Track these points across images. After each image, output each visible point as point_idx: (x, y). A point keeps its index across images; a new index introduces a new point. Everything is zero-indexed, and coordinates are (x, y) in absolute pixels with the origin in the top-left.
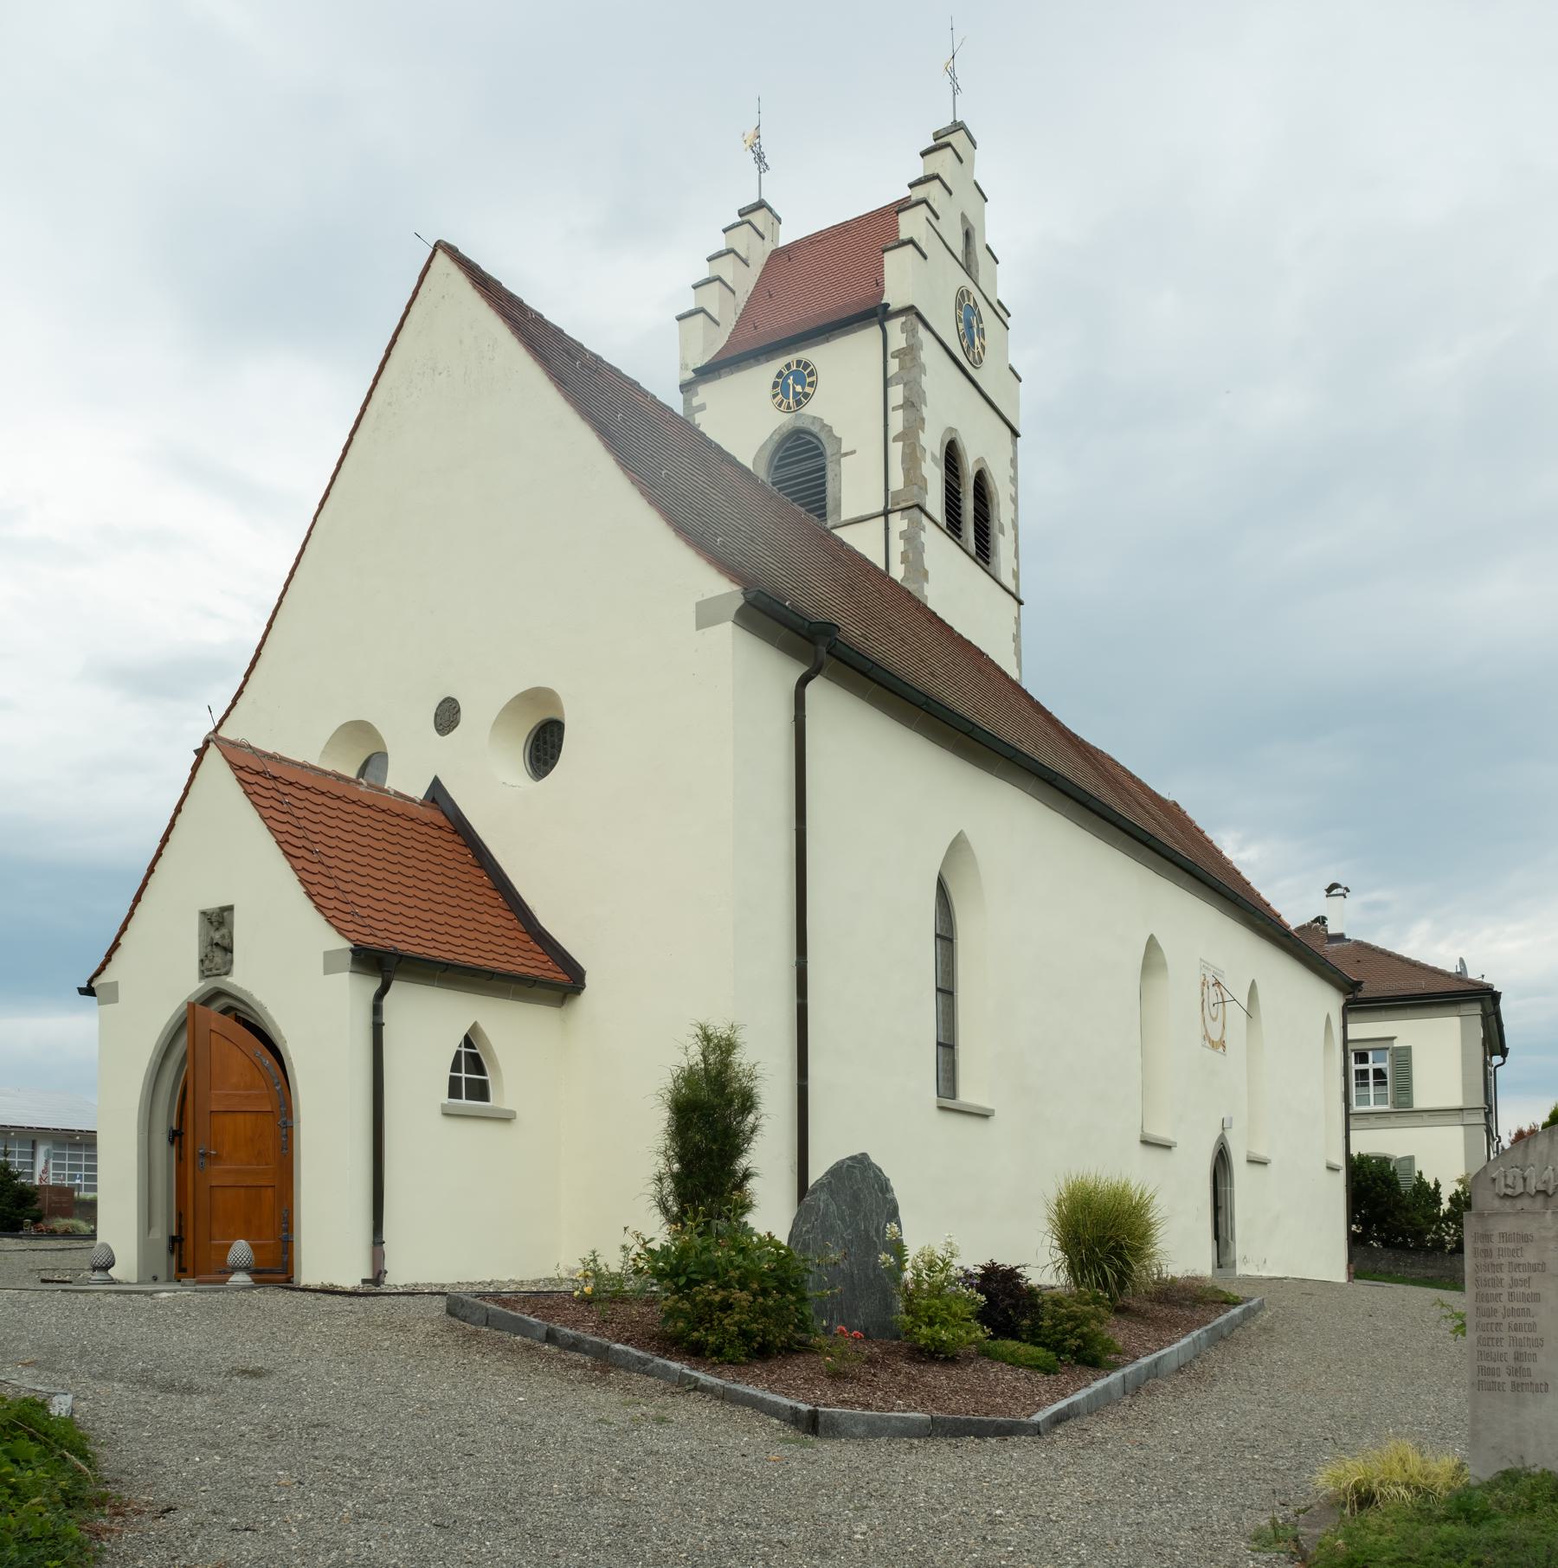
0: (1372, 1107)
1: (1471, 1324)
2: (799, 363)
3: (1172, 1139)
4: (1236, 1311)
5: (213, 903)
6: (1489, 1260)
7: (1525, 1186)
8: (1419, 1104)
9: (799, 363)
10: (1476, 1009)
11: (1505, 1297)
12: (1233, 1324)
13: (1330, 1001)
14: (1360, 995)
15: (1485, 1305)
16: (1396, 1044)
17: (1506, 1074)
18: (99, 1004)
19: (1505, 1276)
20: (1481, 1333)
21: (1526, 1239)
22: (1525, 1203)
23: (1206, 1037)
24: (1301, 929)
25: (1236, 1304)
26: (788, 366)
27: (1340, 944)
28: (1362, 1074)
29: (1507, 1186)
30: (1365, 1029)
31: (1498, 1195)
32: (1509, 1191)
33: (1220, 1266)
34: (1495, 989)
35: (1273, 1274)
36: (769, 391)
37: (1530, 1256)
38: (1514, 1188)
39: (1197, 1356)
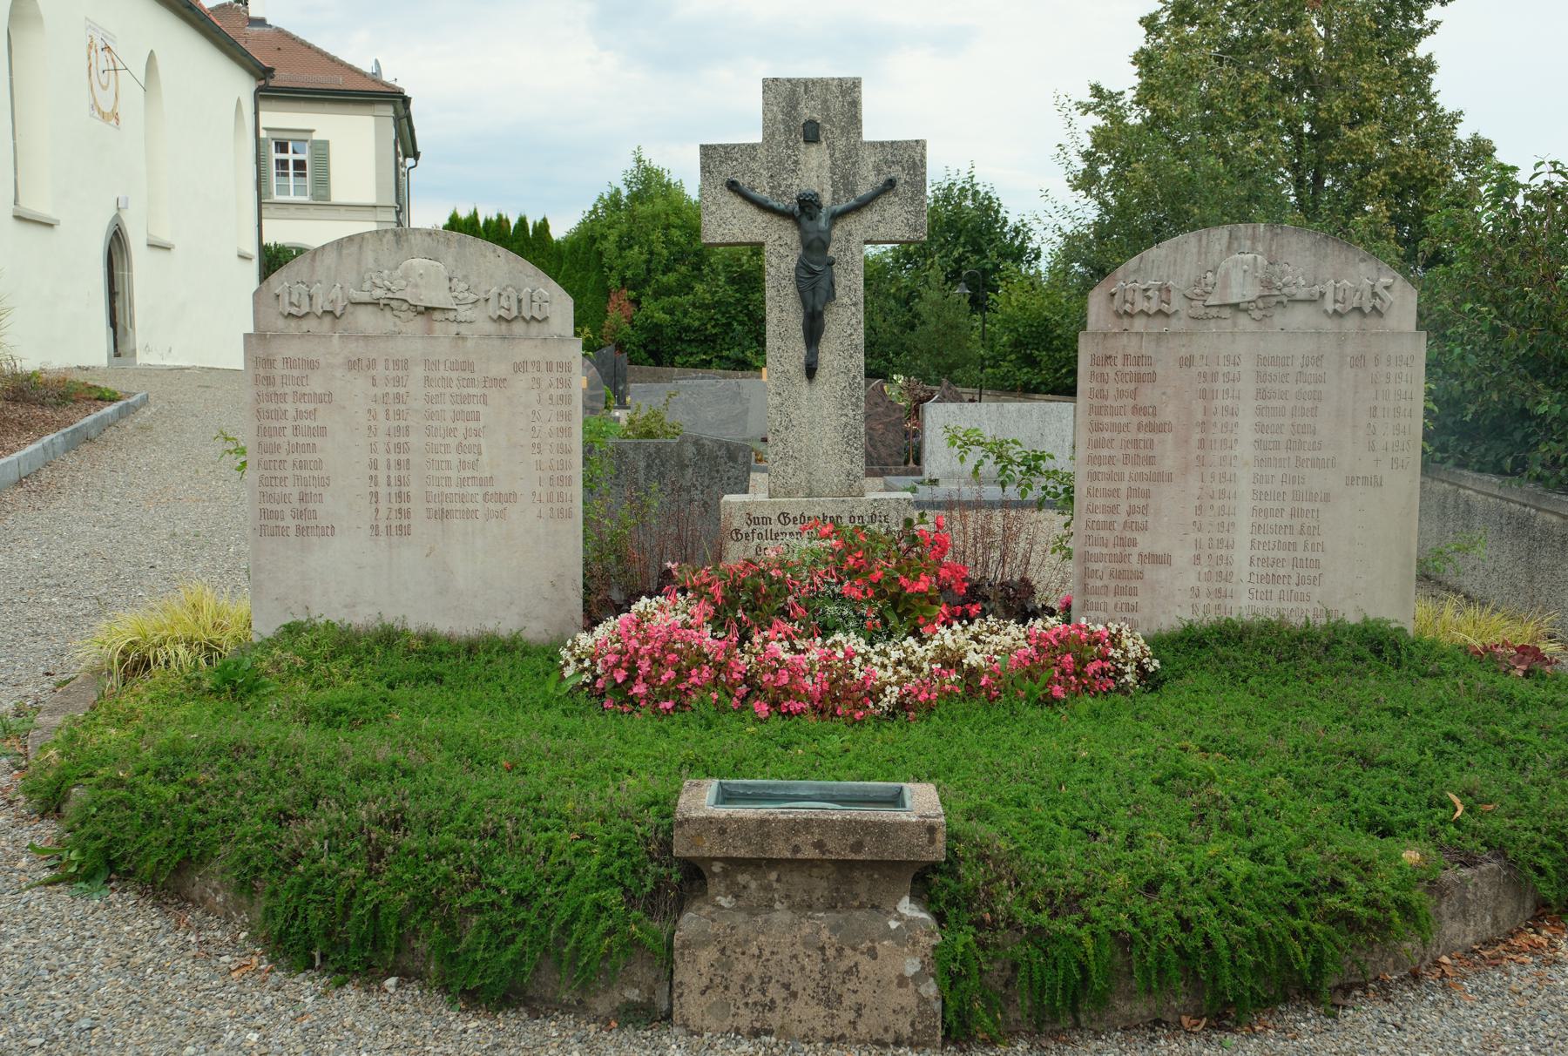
0: (292, 198)
1: (252, 458)
3: (54, 216)
4: (110, 409)
6: (271, 389)
7: (311, 305)
10: (389, 111)
11: (288, 432)
12: (104, 425)
13: (242, 86)
14: (272, 83)
15: (267, 440)
16: (315, 137)
17: (419, 175)
19: (289, 407)
20: (263, 472)
21: (312, 365)
22: (310, 324)
23: (95, 106)
24: (212, 10)
25: (112, 400)
27: (261, 29)
28: (283, 164)
29: (291, 304)
30: (279, 118)
31: (282, 314)
32: (294, 311)
33: (117, 354)
35: (178, 364)
37: (316, 385)
38: (299, 307)
39: (47, 464)
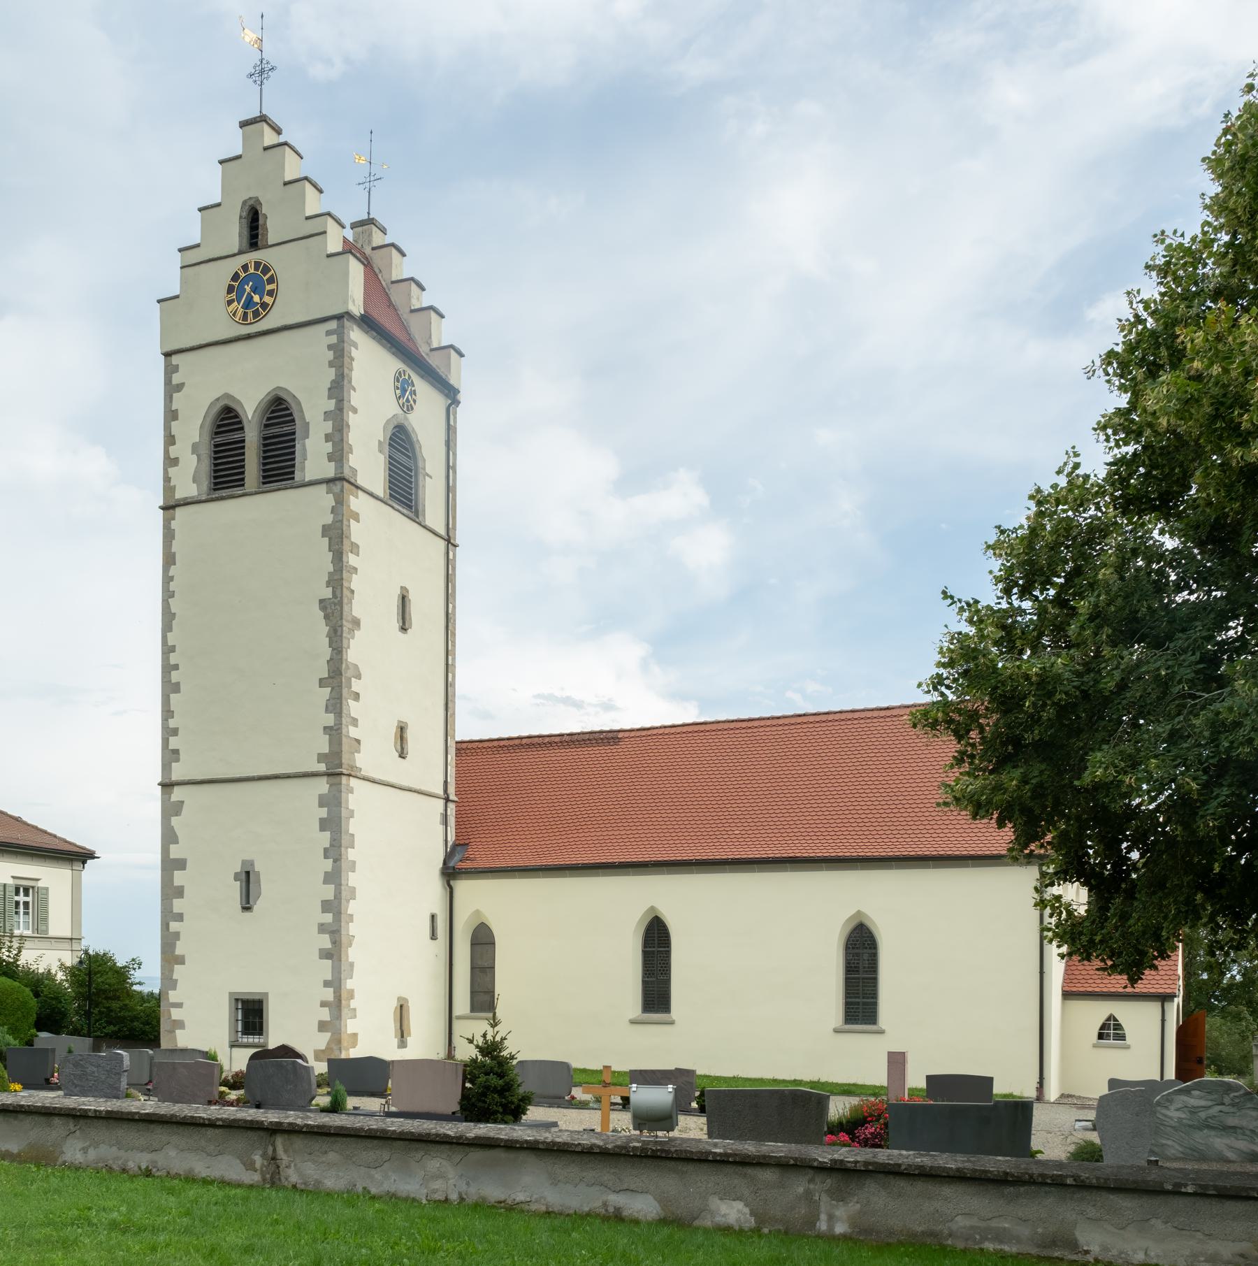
2: (257, 264)
5: (247, 914)
8: (52, 933)
9: (257, 264)
18: (990, 1080)
26: (245, 268)
34: (1214, 189)
36: (222, 294)
